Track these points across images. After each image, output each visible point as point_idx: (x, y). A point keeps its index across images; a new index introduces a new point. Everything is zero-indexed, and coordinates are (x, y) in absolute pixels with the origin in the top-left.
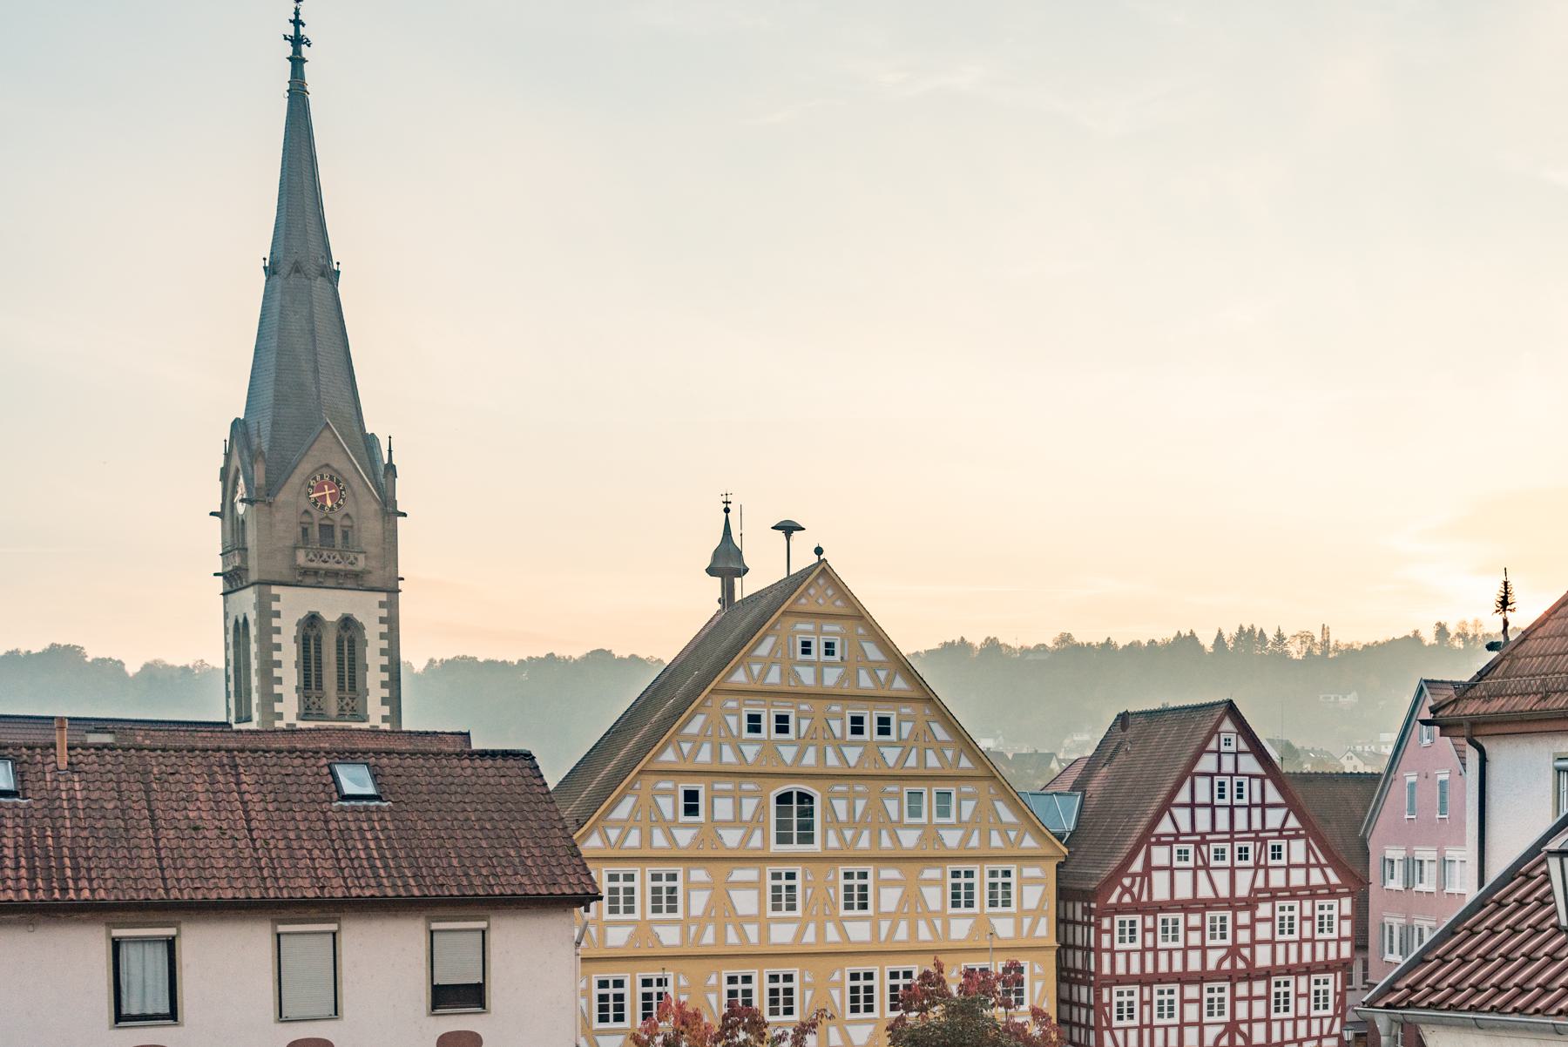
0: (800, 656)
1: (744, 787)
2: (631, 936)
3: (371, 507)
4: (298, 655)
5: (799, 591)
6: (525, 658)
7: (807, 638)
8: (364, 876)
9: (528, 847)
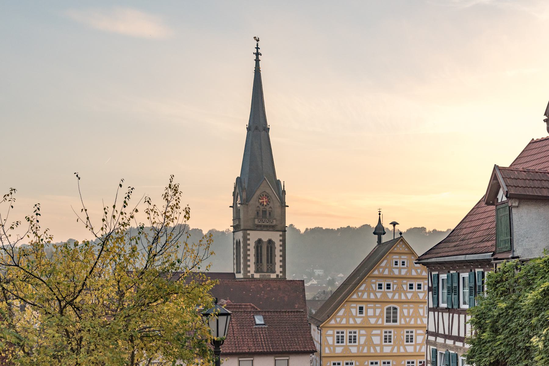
0: (394, 266)
1: (377, 305)
2: (343, 350)
3: (278, 204)
4: (255, 252)
5: (394, 246)
6: (339, 228)
7: (396, 260)
8: (260, 346)
9: (300, 338)
